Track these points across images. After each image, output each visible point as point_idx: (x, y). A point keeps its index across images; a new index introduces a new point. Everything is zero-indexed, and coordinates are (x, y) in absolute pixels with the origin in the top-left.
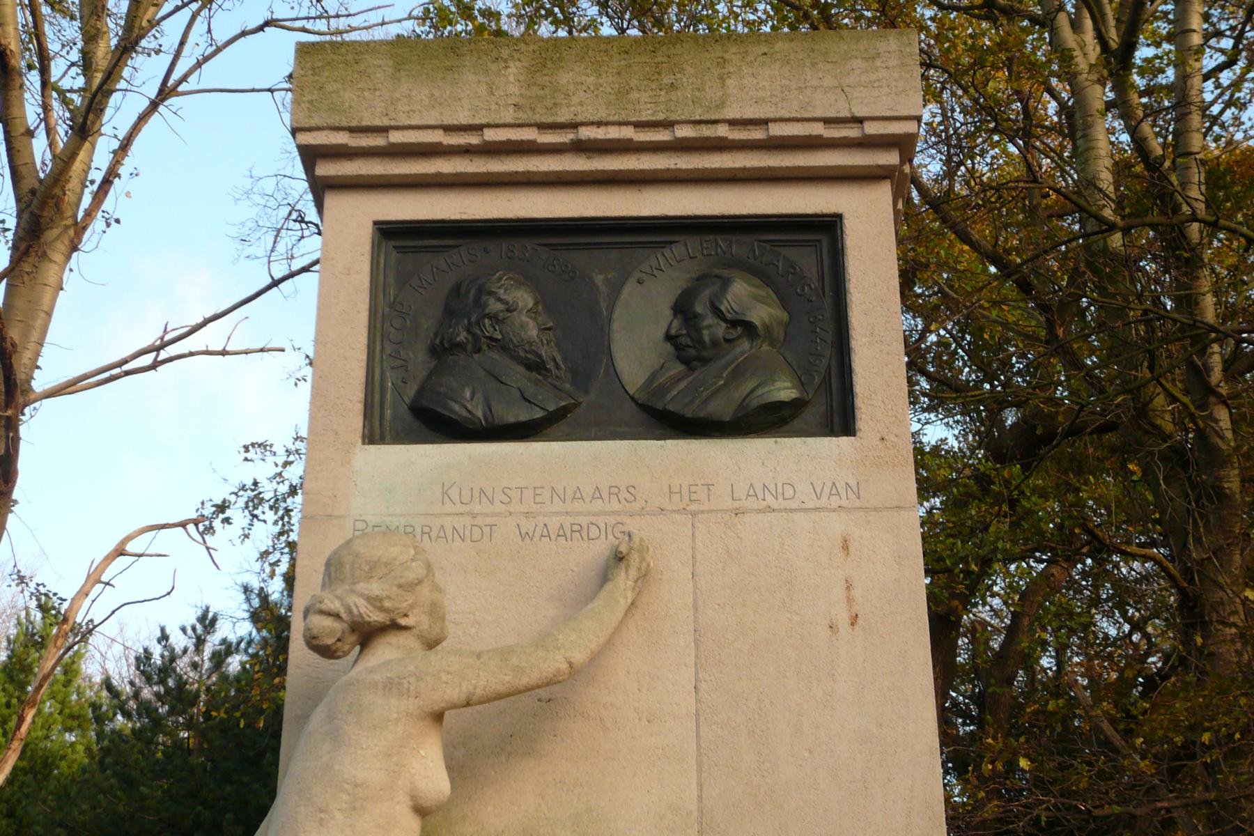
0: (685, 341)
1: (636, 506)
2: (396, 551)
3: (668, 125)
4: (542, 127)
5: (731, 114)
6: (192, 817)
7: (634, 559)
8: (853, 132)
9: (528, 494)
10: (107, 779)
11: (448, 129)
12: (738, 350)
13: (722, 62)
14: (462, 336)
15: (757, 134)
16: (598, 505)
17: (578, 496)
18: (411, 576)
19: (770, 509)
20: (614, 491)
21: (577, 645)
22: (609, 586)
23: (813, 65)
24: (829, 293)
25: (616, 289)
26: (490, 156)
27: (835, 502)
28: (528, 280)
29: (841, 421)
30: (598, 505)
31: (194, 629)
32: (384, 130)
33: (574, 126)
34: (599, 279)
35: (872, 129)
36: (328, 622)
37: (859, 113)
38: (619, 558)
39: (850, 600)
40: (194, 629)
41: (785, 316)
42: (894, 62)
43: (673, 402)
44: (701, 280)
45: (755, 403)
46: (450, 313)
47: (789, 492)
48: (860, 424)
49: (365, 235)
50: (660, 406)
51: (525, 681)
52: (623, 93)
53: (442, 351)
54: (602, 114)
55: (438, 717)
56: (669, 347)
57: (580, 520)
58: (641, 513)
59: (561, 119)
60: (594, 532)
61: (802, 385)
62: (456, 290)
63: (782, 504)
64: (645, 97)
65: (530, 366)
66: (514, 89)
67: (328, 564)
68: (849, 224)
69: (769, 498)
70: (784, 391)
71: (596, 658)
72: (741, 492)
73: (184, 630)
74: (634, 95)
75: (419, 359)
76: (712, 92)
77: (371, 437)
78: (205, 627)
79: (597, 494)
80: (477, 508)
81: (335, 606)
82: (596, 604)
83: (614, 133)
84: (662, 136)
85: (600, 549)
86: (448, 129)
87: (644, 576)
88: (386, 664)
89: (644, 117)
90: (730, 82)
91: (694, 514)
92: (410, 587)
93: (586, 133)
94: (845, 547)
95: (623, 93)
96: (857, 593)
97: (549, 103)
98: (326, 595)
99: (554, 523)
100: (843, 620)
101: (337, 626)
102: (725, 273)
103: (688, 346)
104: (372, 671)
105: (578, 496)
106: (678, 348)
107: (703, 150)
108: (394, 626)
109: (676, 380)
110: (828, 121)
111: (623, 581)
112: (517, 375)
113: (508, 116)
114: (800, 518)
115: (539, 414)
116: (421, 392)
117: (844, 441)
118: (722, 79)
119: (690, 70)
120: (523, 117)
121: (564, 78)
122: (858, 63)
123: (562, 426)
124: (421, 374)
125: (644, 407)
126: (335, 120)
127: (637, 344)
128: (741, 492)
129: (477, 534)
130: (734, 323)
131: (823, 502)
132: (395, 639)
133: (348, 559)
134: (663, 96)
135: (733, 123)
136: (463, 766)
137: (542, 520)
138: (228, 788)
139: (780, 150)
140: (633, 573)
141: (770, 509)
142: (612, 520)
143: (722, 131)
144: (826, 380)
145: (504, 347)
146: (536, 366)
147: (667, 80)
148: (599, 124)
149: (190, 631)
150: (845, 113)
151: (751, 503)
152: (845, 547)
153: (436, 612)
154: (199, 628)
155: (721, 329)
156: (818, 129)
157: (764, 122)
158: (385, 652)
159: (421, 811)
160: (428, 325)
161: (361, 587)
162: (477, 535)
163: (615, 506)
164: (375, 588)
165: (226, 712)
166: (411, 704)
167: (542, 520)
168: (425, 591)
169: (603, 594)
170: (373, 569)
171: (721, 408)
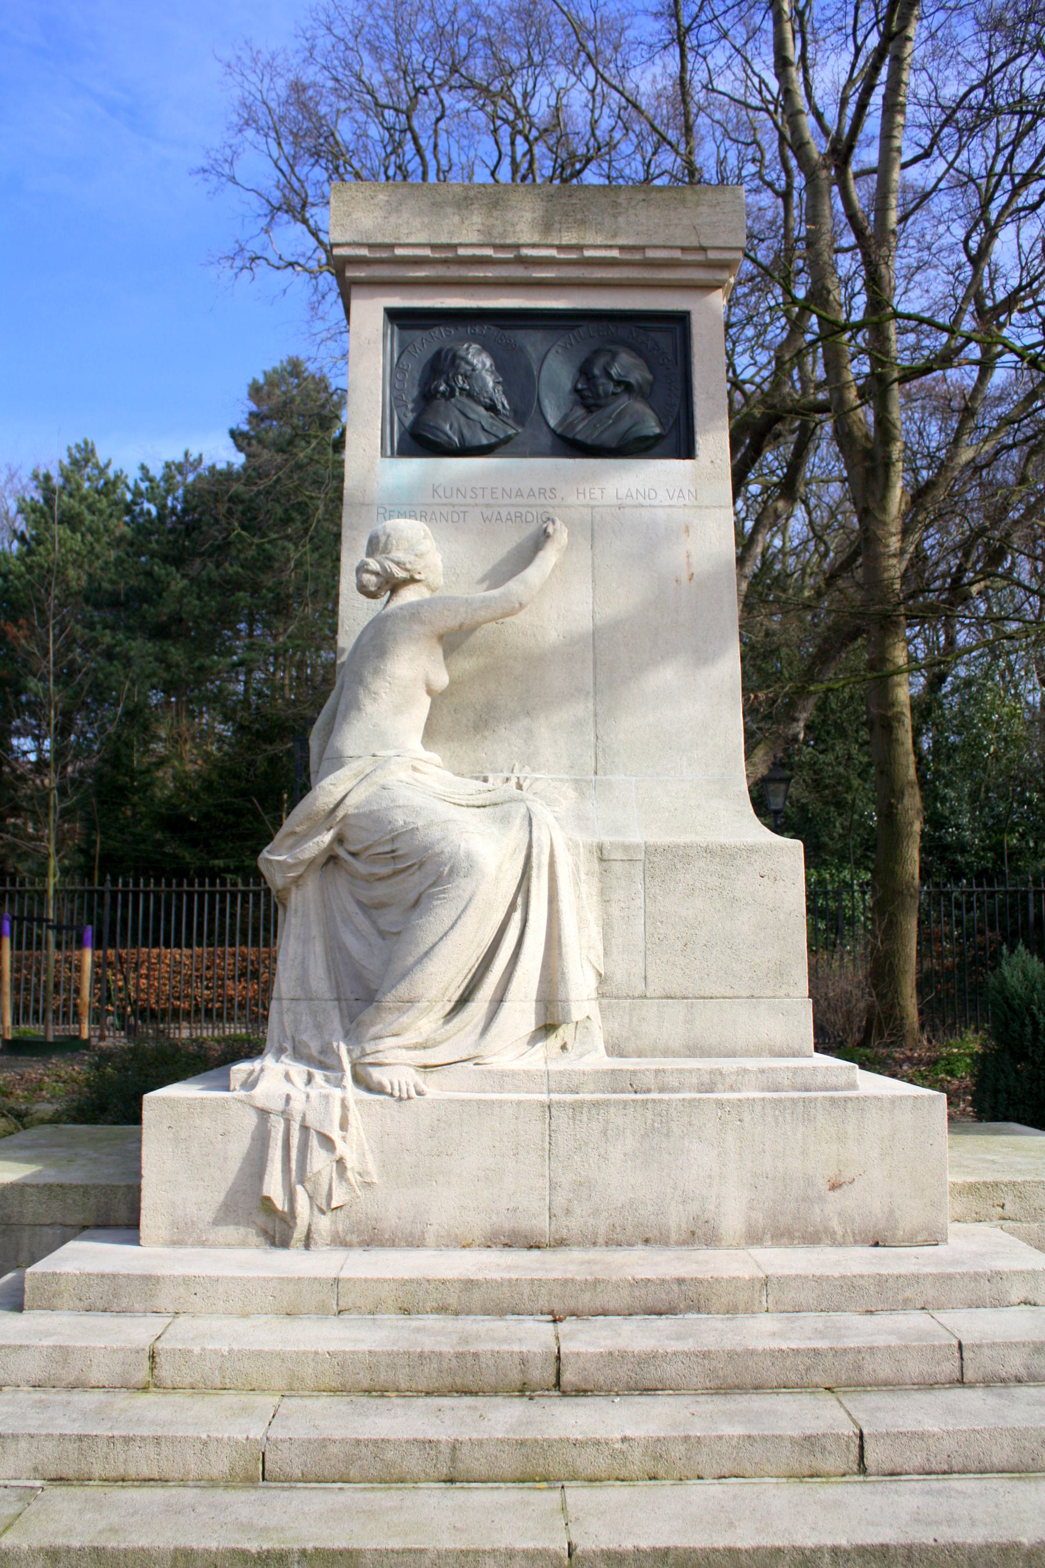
8: (699, 257)
9: (488, 492)
23: (676, 209)
29: (686, 450)
32: (392, 246)
43: (582, 431)
47: (653, 495)
50: (570, 436)
57: (524, 510)
60: (530, 518)
68: (695, 319)
69: (641, 498)
80: (454, 500)
98: (370, 561)
106: (583, 398)
113: (474, 238)
118: (615, 216)
123: (507, 448)
131: (674, 502)
142: (541, 510)
150: (696, 244)
156: (677, 254)
157: (643, 248)
171: (609, 438)
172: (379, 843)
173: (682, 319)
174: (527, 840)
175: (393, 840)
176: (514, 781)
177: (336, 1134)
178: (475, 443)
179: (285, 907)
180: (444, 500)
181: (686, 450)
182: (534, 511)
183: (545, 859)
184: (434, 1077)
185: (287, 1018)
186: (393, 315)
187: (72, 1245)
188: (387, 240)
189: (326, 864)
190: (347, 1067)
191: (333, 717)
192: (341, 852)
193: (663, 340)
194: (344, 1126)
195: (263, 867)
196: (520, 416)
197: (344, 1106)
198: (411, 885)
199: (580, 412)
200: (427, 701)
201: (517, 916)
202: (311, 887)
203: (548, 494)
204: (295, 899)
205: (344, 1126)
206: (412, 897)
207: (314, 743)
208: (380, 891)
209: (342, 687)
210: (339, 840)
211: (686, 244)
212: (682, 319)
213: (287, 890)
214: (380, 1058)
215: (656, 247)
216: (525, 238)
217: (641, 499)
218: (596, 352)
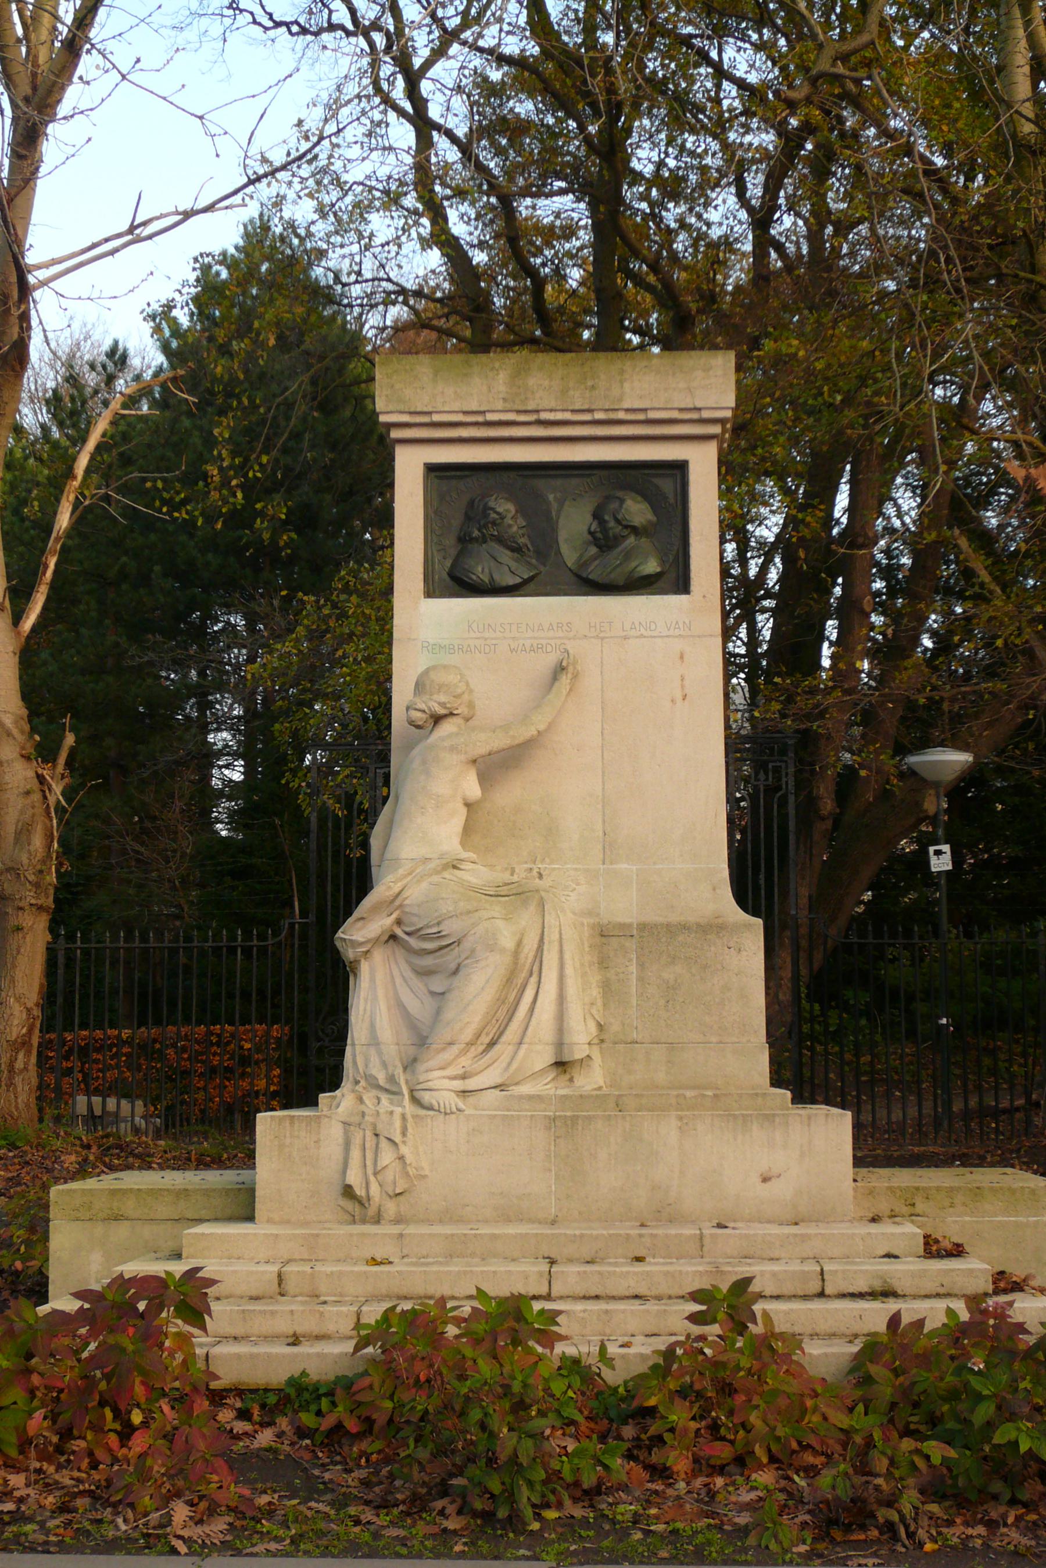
0: (599, 535)
1: (571, 634)
2: (451, 678)
3: (590, 411)
4: (519, 412)
5: (626, 406)
6: (117, 568)
7: (571, 669)
8: (695, 416)
9: (514, 627)
10: (27, 530)
11: (465, 413)
12: (628, 542)
13: (622, 372)
14: (476, 533)
15: (641, 417)
16: (551, 634)
17: (541, 628)
18: (459, 691)
19: (642, 636)
20: (560, 626)
21: (540, 722)
22: (557, 684)
23: (674, 374)
24: (680, 507)
25: (561, 503)
26: (489, 429)
27: (677, 632)
28: (512, 497)
29: (682, 585)
30: (551, 634)
31: (104, 367)
32: (430, 413)
33: (537, 411)
34: (551, 497)
35: (706, 414)
36: (419, 714)
37: (699, 405)
38: (560, 669)
39: (683, 686)
40: (104, 367)
41: (654, 519)
42: (720, 372)
43: (594, 573)
44: (608, 498)
45: (636, 575)
46: (468, 518)
47: (653, 627)
48: (692, 588)
49: (420, 471)
50: (584, 575)
51: (517, 742)
52: (564, 391)
53: (464, 540)
54: (553, 404)
55: (474, 761)
56: (590, 538)
57: (544, 642)
58: (574, 638)
59: (530, 408)
60: (549, 649)
61: (662, 562)
62: (471, 504)
63: (650, 633)
64: (577, 394)
65: (513, 550)
66: (502, 388)
67: (417, 684)
68: (692, 468)
69: (643, 631)
70: (652, 566)
71: (550, 726)
72: (627, 626)
73: (92, 367)
74: (571, 393)
75: (450, 541)
76: (616, 391)
77: (429, 594)
78: (116, 364)
79: (551, 627)
80: (487, 635)
81: (423, 706)
82: (550, 696)
83: (559, 416)
84: (587, 417)
85: (551, 659)
86: (465, 413)
87: (576, 676)
88: (450, 736)
89: (577, 407)
90: (627, 385)
91: (602, 639)
92: (458, 697)
93: (544, 416)
94: (682, 657)
95: (564, 391)
96: (687, 682)
97: (523, 397)
98: (417, 700)
99: (528, 643)
100: (679, 696)
101: (424, 716)
102: (620, 494)
103: (604, 540)
104: (443, 739)
105: (541, 628)
106: (595, 539)
107: (609, 426)
108: (452, 714)
109: (594, 558)
110: (681, 410)
111: (565, 680)
112: (506, 556)
113: (500, 405)
114: (659, 640)
115: (518, 580)
116: (454, 565)
117: (684, 597)
118: (622, 382)
119: (603, 377)
120: (508, 406)
121: (531, 382)
122: (699, 373)
123: (532, 586)
124: (453, 552)
125: (578, 576)
126: (401, 407)
127: (574, 524)
128: (627, 626)
129: (487, 650)
130: (626, 527)
131: (671, 633)
132: (451, 720)
133: (428, 683)
134: (587, 394)
135: (627, 410)
136: (484, 779)
137: (521, 642)
138: (153, 537)
139: (654, 427)
140: (570, 676)
141: (642, 636)
142: (558, 642)
143: (621, 415)
144: (677, 557)
145: (500, 540)
146: (517, 550)
147: (590, 383)
148: (551, 410)
149: (100, 369)
150: (691, 406)
151: (633, 633)
152: (682, 657)
153: (471, 705)
154: (111, 367)
155: (618, 529)
156: (676, 415)
157: (645, 410)
158: (447, 728)
159: (468, 805)
160: (456, 522)
161: (435, 697)
162: (487, 650)
163: (560, 634)
164: (443, 698)
165: (187, 513)
166: (463, 757)
167: (521, 642)
168: (466, 697)
169: (554, 689)
170: (441, 687)
171: (618, 577)
172: (428, 926)
173: (680, 468)
174: (539, 932)
175: (439, 924)
176: (535, 871)
177: (398, 1139)
178: (504, 584)
179: (355, 975)
180: (479, 635)
181: (682, 585)
182: (553, 642)
183: (556, 936)
184: (471, 1100)
185: (360, 1061)
186: (433, 470)
187: (412, 128)
188: (425, 409)
189: (387, 941)
190: (405, 1092)
191: (391, 823)
192: (399, 932)
193: (667, 485)
194: (404, 1134)
195: (338, 944)
196: (542, 555)
197: (404, 1117)
198: (450, 959)
199: (593, 550)
200: (464, 811)
201: (534, 980)
202: (379, 956)
203: (565, 628)
204: (364, 967)
205: (404, 1134)
206: (453, 966)
207: (375, 842)
208: (428, 961)
209: (397, 798)
210: (399, 922)
211: (683, 406)
212: (680, 468)
213: (357, 962)
214: (430, 1085)
215: (659, 409)
216: (546, 404)
217: (643, 631)
218: (608, 498)
